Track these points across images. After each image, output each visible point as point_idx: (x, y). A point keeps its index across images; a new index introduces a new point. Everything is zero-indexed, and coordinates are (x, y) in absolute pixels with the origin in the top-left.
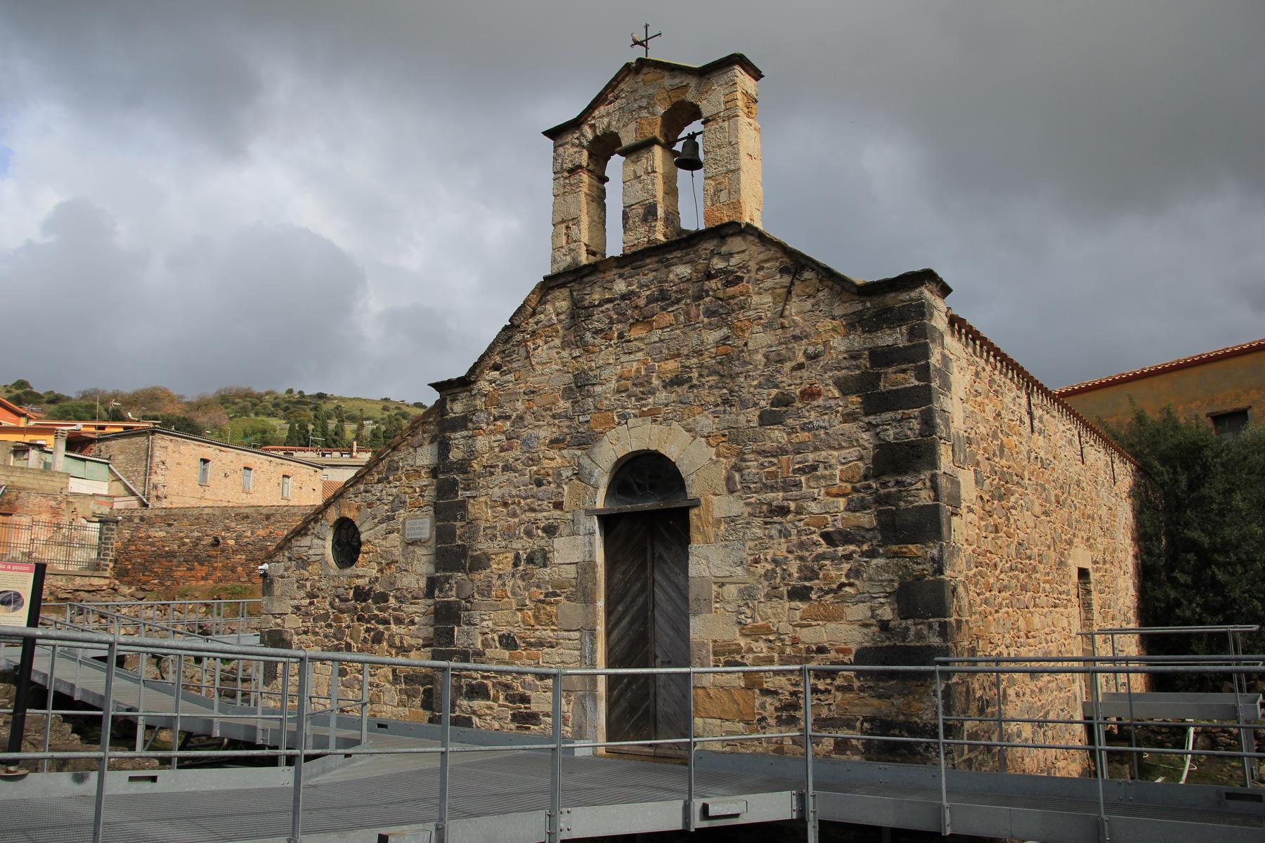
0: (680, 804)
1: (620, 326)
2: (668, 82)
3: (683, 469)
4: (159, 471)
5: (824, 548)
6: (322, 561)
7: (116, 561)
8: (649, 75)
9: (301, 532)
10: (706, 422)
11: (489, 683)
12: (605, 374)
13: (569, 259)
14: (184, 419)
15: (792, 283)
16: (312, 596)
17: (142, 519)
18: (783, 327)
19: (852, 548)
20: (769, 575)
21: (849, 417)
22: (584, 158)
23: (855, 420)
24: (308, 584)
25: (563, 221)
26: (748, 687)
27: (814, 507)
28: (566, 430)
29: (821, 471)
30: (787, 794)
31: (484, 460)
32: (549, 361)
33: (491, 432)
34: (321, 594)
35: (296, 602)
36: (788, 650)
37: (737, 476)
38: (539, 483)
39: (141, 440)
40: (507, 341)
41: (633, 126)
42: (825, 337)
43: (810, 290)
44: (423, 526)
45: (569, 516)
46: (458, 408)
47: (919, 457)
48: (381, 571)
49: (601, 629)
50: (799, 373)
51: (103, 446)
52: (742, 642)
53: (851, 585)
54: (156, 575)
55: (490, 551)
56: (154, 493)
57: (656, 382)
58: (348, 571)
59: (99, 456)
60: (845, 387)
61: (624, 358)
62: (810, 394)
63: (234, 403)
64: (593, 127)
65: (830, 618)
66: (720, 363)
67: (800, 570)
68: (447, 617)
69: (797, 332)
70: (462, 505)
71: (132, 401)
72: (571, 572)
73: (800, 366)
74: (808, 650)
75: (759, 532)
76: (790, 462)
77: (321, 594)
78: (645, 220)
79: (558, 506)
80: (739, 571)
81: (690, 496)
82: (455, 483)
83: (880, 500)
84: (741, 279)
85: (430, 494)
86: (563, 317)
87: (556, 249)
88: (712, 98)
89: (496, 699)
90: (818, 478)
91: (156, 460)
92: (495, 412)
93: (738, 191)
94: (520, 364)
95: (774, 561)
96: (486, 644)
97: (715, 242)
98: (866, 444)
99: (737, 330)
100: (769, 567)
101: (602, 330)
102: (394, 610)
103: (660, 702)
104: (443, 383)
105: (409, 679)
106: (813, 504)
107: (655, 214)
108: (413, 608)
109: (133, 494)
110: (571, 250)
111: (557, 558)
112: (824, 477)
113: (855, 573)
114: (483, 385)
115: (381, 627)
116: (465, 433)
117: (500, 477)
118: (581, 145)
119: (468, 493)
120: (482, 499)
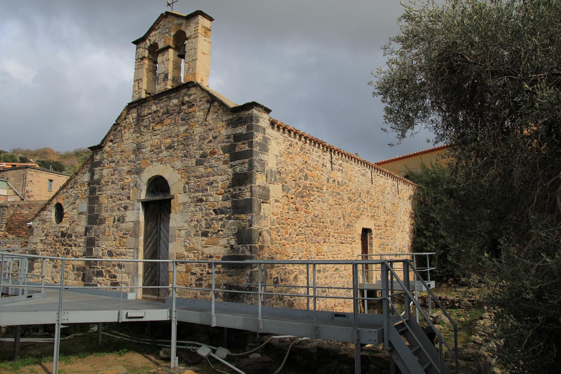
0: (118, 312)
1: (153, 124)
2: (176, 22)
3: (170, 183)
4: (29, 185)
5: (214, 216)
6: (51, 221)
7: (7, 224)
8: (170, 19)
9: (44, 209)
10: (178, 164)
11: (103, 270)
12: (147, 144)
13: (138, 96)
14: (56, 162)
15: (210, 107)
16: (47, 235)
17: (18, 206)
18: (206, 125)
19: (223, 215)
20: (195, 226)
21: (225, 162)
22: (146, 54)
23: (227, 163)
24: (46, 230)
25: (137, 80)
26: (187, 272)
27: (211, 199)
28: (133, 167)
29: (215, 185)
30: (167, 310)
31: (106, 179)
32: (129, 137)
33: (108, 168)
34: (50, 235)
35: (41, 238)
36: (200, 257)
37: (187, 186)
38: (123, 189)
39: (21, 171)
40: (115, 130)
41: (163, 40)
42: (220, 129)
43: (216, 110)
44: (84, 206)
45: (132, 202)
46: (98, 158)
47: (247, 179)
48: (70, 225)
49: (141, 248)
50: (210, 144)
51: (4, 174)
52: (186, 253)
53: (222, 231)
54: (24, 230)
55: (106, 216)
56: (27, 194)
57: (163, 147)
58: (59, 225)
59: (3, 178)
60: (225, 150)
61: (153, 137)
62: (213, 153)
63: (82, 155)
64: (150, 40)
65: (215, 244)
66: (184, 140)
67: (206, 225)
68: (91, 243)
69: (210, 127)
70: (97, 198)
71: (34, 154)
72: (131, 225)
73: (210, 141)
74: (207, 257)
75: (193, 209)
76: (204, 180)
77: (50, 235)
78: (164, 80)
79: (129, 198)
80: (186, 225)
81: (171, 194)
82: (95, 189)
83: (234, 196)
84: (193, 105)
85: (88, 192)
86: (134, 120)
87: (134, 92)
88: (190, 29)
89: (105, 277)
90: (213, 187)
91: (28, 180)
92: (110, 159)
93: (195, 69)
94: (119, 139)
95: (197, 221)
96: (103, 255)
97: (186, 90)
98: (230, 173)
99: (191, 126)
100: (196, 223)
101: (147, 126)
102: (74, 241)
103: (161, 278)
104: (95, 147)
105: (78, 269)
106: (211, 198)
107: (167, 78)
108: (80, 240)
109: (18, 195)
110: (139, 92)
111: (127, 219)
112: (215, 187)
113: (223, 226)
114: (107, 148)
115: (69, 248)
116: (100, 168)
117: (110, 186)
118: (145, 48)
119: (100, 193)
120: (104, 195)
